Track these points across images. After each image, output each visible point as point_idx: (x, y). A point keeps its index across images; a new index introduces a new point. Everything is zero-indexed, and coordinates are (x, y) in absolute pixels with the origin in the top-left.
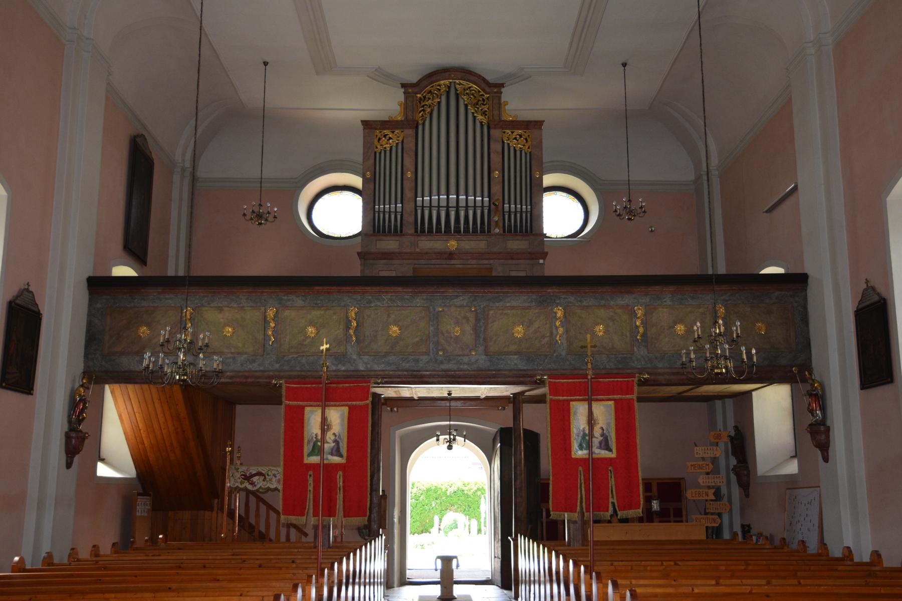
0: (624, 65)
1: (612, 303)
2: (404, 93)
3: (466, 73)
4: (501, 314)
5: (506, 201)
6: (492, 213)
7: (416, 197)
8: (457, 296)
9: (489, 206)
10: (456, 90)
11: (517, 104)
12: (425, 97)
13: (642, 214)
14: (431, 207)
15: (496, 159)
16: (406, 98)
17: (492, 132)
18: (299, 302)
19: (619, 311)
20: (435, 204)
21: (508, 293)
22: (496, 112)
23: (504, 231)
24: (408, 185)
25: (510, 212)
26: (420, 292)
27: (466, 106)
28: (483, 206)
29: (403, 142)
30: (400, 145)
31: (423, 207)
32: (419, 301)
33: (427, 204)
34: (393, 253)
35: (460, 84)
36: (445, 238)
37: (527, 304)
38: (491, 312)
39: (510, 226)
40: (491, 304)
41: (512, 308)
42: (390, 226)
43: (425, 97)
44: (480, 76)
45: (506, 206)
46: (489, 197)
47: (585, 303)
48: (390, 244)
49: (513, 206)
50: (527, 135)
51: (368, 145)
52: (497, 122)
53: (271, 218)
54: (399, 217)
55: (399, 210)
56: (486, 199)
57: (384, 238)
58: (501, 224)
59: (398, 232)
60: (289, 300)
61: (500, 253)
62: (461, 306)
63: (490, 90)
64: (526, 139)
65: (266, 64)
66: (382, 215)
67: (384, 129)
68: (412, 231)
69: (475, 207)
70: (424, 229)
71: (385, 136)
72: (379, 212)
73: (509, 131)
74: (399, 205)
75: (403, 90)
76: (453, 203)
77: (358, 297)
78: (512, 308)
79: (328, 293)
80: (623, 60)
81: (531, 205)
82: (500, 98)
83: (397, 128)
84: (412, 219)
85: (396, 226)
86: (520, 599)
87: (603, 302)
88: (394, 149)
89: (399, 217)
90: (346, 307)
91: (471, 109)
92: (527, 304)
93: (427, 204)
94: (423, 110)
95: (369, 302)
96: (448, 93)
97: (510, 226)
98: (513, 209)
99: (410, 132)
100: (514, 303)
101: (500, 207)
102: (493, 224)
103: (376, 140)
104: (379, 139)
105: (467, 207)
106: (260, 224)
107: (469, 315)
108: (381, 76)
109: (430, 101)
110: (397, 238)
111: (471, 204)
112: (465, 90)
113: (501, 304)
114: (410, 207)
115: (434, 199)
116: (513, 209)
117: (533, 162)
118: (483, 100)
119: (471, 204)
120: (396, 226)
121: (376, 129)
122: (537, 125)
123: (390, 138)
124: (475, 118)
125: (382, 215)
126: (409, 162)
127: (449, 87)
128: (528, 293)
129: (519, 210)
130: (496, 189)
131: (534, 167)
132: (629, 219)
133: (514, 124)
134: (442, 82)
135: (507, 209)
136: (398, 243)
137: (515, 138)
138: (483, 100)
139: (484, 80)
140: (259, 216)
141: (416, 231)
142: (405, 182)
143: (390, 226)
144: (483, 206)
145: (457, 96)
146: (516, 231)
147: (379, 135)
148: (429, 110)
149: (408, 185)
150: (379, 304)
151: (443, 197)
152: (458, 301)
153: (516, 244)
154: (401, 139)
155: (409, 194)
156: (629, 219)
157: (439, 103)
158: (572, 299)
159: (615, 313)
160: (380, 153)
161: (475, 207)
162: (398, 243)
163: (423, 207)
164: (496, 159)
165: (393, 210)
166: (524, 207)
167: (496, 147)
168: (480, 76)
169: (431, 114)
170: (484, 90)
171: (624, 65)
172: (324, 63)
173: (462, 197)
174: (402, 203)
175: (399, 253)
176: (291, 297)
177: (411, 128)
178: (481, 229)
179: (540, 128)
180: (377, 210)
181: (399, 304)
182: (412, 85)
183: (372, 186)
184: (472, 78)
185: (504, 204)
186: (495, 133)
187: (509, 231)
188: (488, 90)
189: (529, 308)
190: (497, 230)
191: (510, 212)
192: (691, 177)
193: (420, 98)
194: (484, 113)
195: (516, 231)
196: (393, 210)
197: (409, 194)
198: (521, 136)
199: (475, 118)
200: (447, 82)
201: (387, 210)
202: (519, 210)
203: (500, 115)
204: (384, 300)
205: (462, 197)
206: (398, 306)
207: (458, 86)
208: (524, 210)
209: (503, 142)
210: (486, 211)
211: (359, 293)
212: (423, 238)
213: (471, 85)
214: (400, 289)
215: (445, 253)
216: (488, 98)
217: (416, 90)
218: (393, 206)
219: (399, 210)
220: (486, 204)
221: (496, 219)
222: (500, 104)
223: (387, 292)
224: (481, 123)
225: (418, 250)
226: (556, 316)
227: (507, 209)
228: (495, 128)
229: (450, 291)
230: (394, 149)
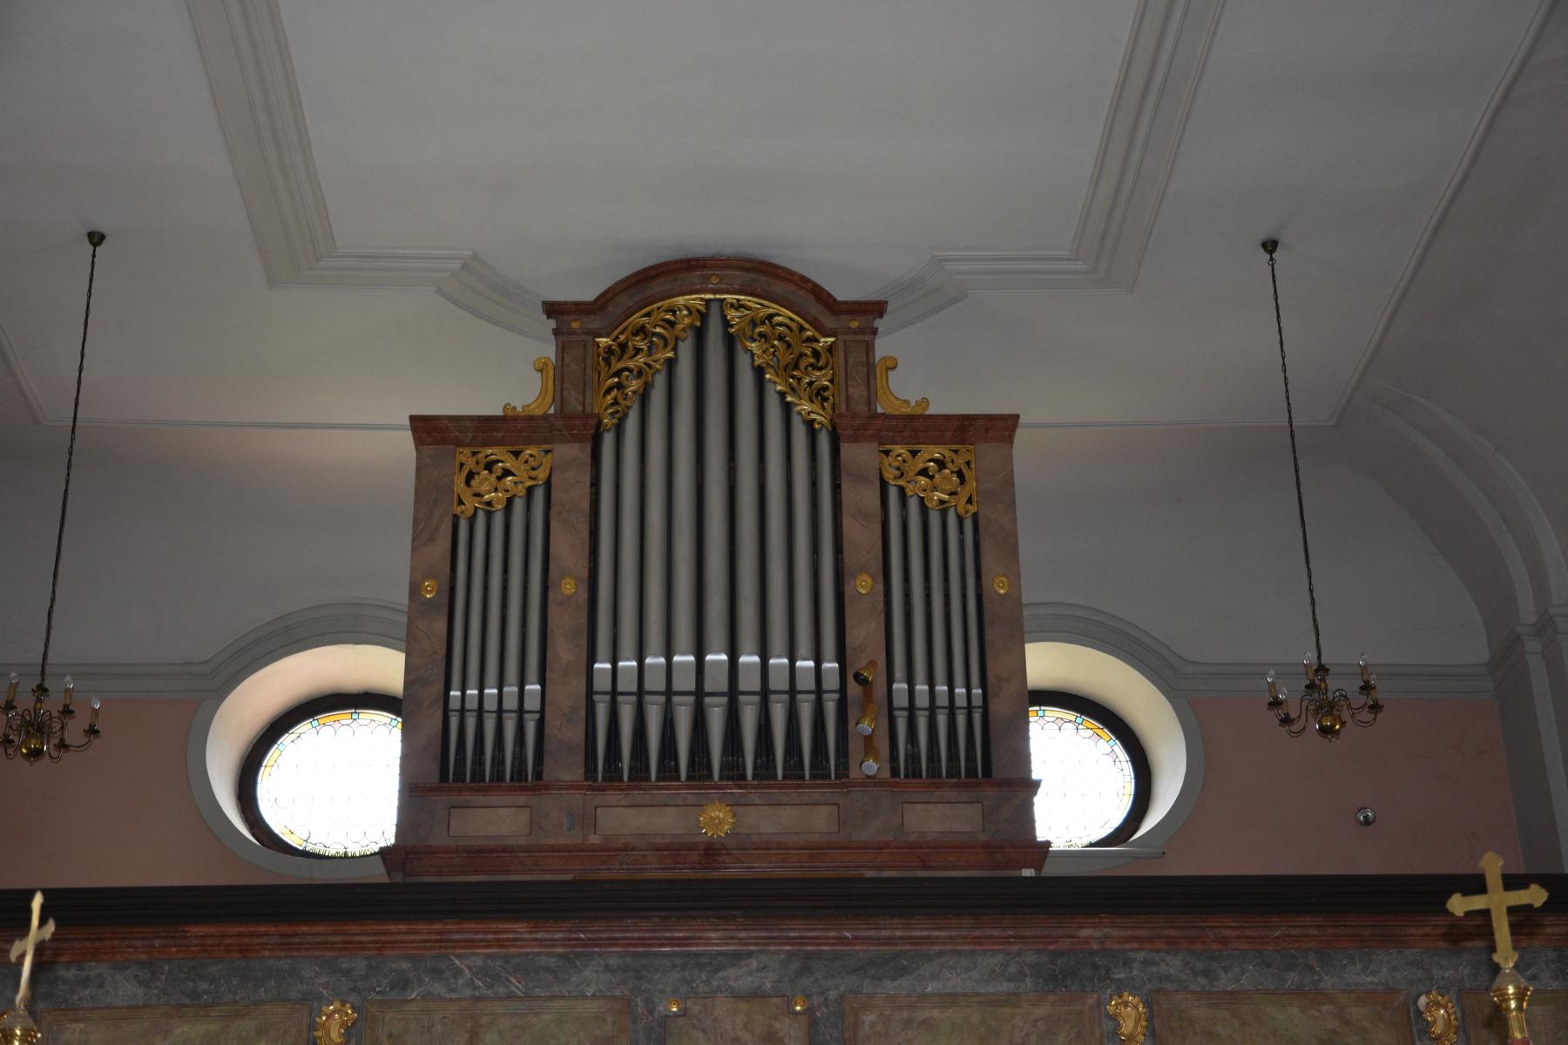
0: (1270, 246)
1: (1328, 982)
2: (556, 332)
3: (760, 273)
4: (908, 1023)
5: (899, 671)
6: (853, 713)
7: (592, 658)
8: (737, 957)
9: (843, 690)
10: (727, 324)
11: (922, 373)
12: (623, 347)
13: (1366, 716)
14: (641, 692)
15: (861, 536)
16: (562, 350)
17: (846, 450)
18: (125, 988)
19: (1356, 1012)
20: (655, 682)
21: (930, 940)
22: (858, 392)
23: (895, 772)
24: (566, 622)
25: (912, 709)
26: (596, 943)
27: (759, 372)
28: (819, 691)
29: (548, 484)
30: (539, 495)
31: (614, 693)
32: (592, 977)
33: (627, 683)
34: (505, 850)
35: (739, 306)
36: (688, 795)
37: (1006, 987)
38: (869, 1018)
39: (913, 758)
40: (868, 987)
41: (949, 999)
42: (498, 761)
43: (623, 347)
44: (804, 280)
45: (900, 686)
46: (841, 657)
47: (1225, 982)
48: (498, 821)
49: (922, 687)
50: (960, 461)
51: (429, 492)
52: (862, 422)
53: (75, 734)
54: (531, 728)
55: (532, 704)
56: (830, 665)
57: (479, 799)
58: (883, 746)
59: (526, 777)
60: (85, 982)
61: (882, 847)
62: (755, 995)
63: (834, 328)
64: (960, 474)
65: (96, 239)
66: (471, 722)
67: (487, 444)
68: (576, 773)
69: (793, 691)
70: (614, 765)
71: (489, 467)
72: (463, 711)
73: (900, 450)
74: (533, 687)
75: (552, 323)
76: (717, 682)
77: (359, 965)
78: (949, 999)
79: (244, 950)
80: (1264, 233)
81: (984, 685)
82: (869, 348)
83: (529, 442)
84: (576, 734)
85: (519, 759)
86: (489, 1038)
87: (1292, 978)
88: (519, 505)
89: (531, 728)
90: (311, 1001)
91: (775, 384)
92: (1006, 987)
93: (627, 683)
94: (619, 386)
95: (402, 984)
96: (700, 335)
97: (913, 758)
98: (922, 701)
99: (573, 452)
100: (954, 982)
101: (880, 691)
102: (855, 747)
103: (459, 484)
104: (470, 476)
105: (765, 693)
106: (36, 754)
107: (784, 1027)
108: (476, 288)
109: (641, 359)
110: (522, 799)
111: (779, 682)
112: (754, 323)
113: (905, 983)
114: (568, 693)
115: (653, 665)
116: (922, 701)
117: (985, 547)
118: (816, 354)
119: (779, 682)
120: (519, 759)
121: (459, 443)
122: (1002, 427)
123: (507, 472)
124: (787, 408)
125: (471, 722)
126: (568, 550)
127: (704, 317)
128: (1006, 941)
129: (942, 701)
130: (865, 632)
131: (988, 562)
132: (1325, 731)
133: (919, 427)
134: (681, 300)
135: (901, 700)
136: (524, 816)
137: (924, 472)
138: (816, 354)
139: (818, 293)
140: (36, 727)
141: (590, 771)
142: (553, 611)
143: (498, 761)
144: (819, 691)
145: (730, 342)
146: (934, 772)
147: (470, 464)
148: (634, 385)
149: (566, 622)
150: (438, 988)
151: (684, 659)
152: (742, 977)
153: (938, 818)
154: (542, 474)
155: (565, 651)
156: (1325, 731)
157: (671, 364)
158: (1173, 965)
159: (1347, 1023)
160: (472, 520)
161: (793, 691)
162: (524, 816)
163: (614, 693)
164: (861, 536)
165: (511, 703)
166: (960, 691)
167: (861, 496)
168: (803, 282)
169: (644, 396)
170: (816, 324)
171: (1270, 246)
172: (295, 245)
173: (749, 659)
174: (542, 681)
175: (529, 850)
176: (95, 969)
177: (576, 439)
178: (817, 762)
179: (1009, 439)
180: (455, 704)
181: (518, 987)
182: (580, 309)
183: (441, 626)
184: (778, 288)
185: (890, 680)
186: (859, 454)
187: (915, 772)
188: (829, 322)
189: (1011, 999)
190: (871, 767)
191: (912, 709)
192: (1476, 651)
193: (609, 350)
194: (819, 395)
195: (934, 772)
196: (511, 703)
197: (565, 651)
198: (941, 464)
199: (787, 408)
200: (694, 300)
201: (491, 705)
202: (942, 701)
203: (870, 401)
204: (457, 973)
205: (749, 659)
206: (511, 997)
207: (732, 314)
208: (961, 701)
209: (884, 485)
210: (830, 707)
211: (362, 946)
212: (613, 797)
213: (775, 308)
214: (520, 928)
215: (691, 847)
216: (830, 349)
217: (595, 323)
218: (511, 690)
219: (532, 704)
220: (831, 683)
221: (866, 727)
222: (870, 366)
223: (470, 944)
224: (810, 424)
225: (594, 839)
226: (1115, 1033)
227: (901, 700)
228: (856, 439)
229: (713, 939)
230: (519, 505)
